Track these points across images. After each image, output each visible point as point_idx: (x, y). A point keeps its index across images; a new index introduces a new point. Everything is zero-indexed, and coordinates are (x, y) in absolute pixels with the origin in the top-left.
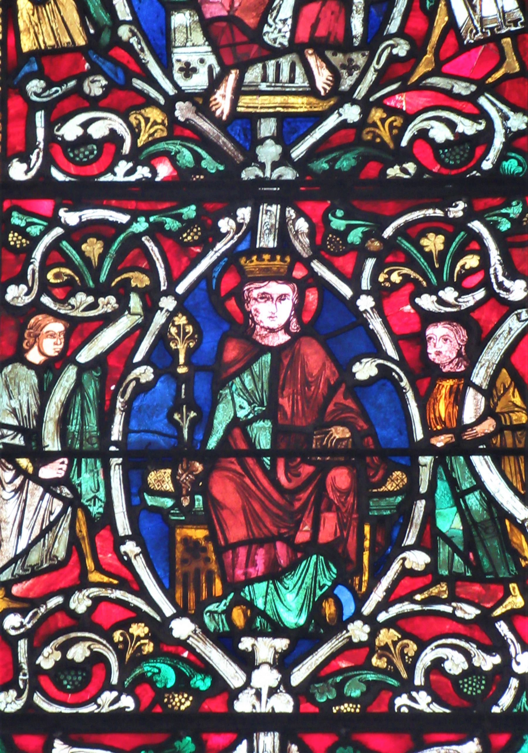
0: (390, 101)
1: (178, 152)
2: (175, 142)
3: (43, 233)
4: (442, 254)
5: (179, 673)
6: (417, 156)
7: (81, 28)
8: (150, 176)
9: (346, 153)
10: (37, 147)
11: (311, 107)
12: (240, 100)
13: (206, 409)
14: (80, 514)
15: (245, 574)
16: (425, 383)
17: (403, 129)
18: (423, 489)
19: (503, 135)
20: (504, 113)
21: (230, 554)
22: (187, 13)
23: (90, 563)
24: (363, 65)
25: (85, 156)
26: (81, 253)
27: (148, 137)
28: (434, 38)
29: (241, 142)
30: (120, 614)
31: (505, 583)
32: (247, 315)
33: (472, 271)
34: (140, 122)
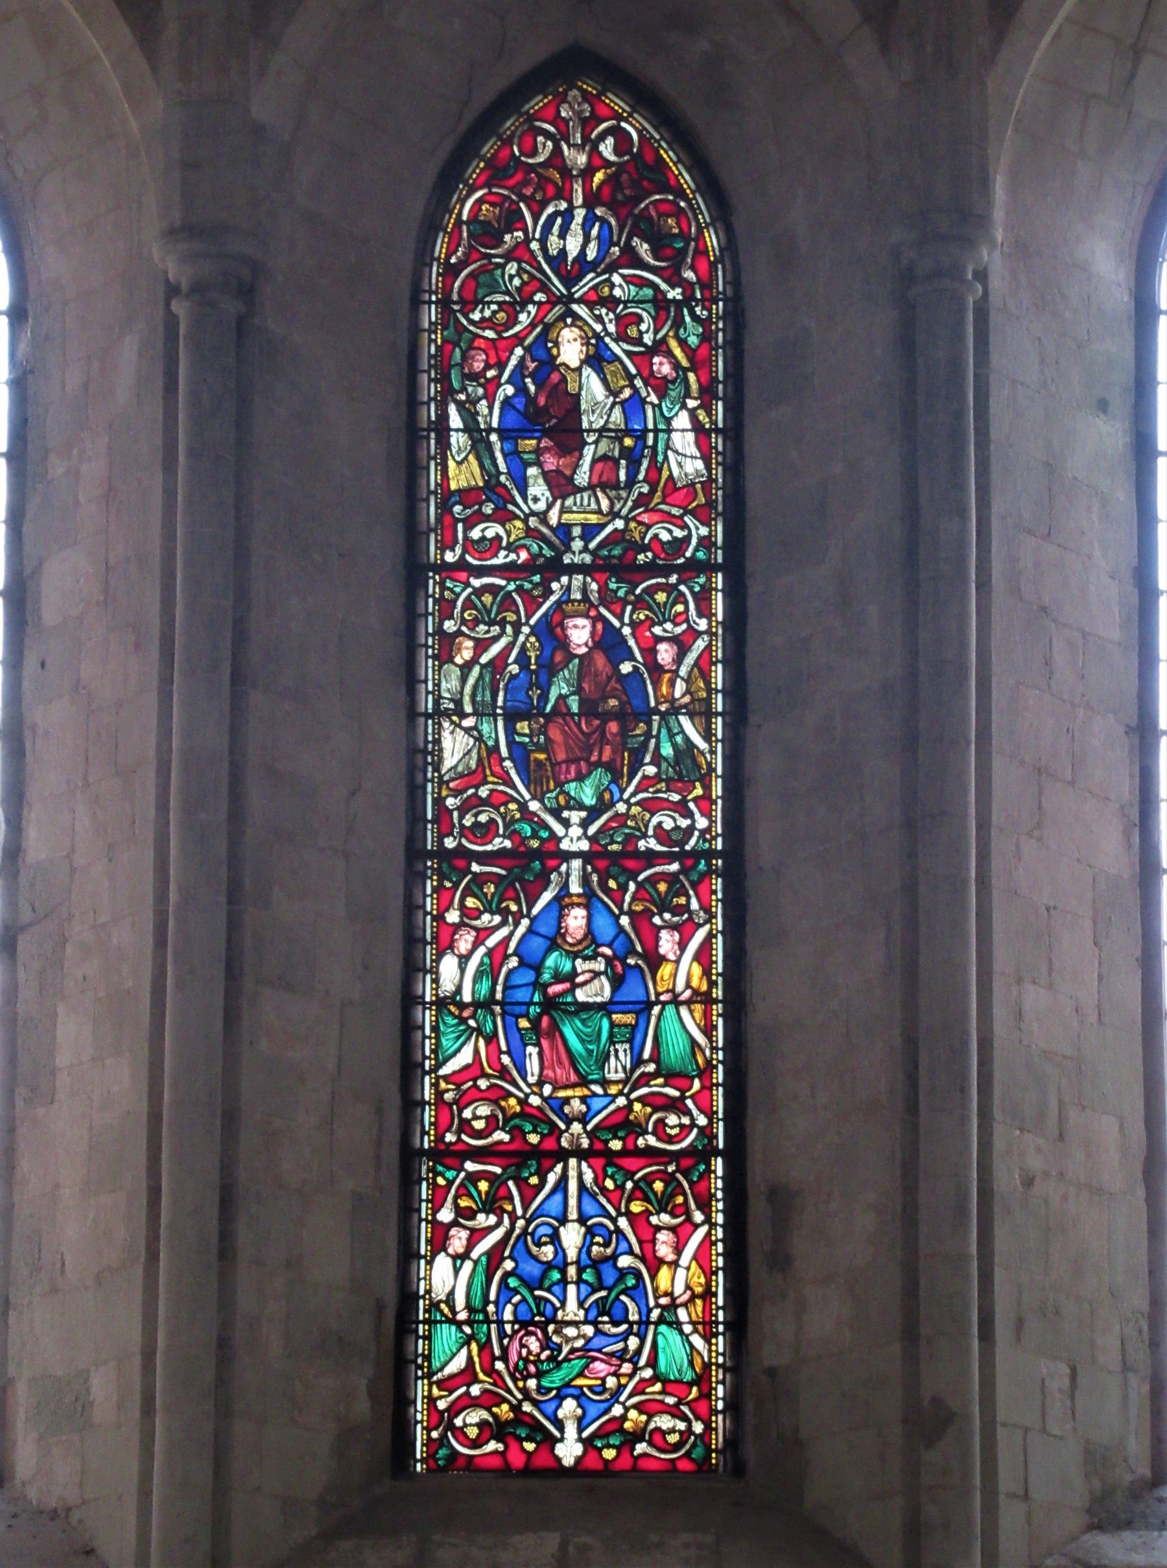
4: (665, 603)
5: (533, 829)
13: (545, 689)
14: (483, 746)
15: (566, 778)
16: (656, 675)
17: (646, 533)
18: (654, 733)
21: (558, 767)
23: (488, 772)
26: (481, 602)
28: (662, 484)
30: (503, 798)
31: (693, 782)
32: (566, 637)
33: (680, 614)
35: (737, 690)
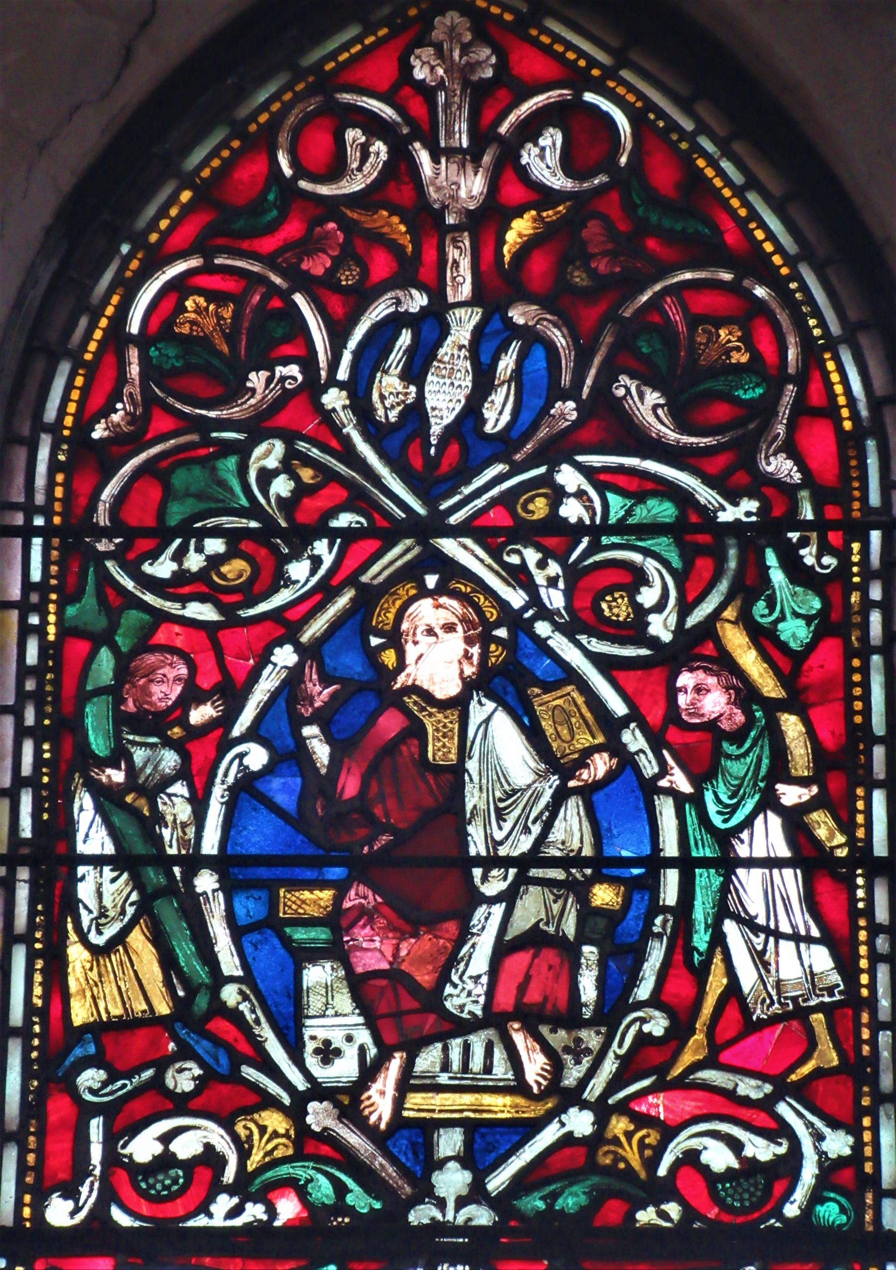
0: (640, 1105)
1: (309, 1181)
2: (306, 1164)
6: (683, 1192)
7: (164, 989)
8: (265, 1217)
9: (572, 1184)
10: (90, 1174)
11: (517, 1112)
12: (408, 1098)
17: (660, 1150)
19: (815, 1164)
20: (816, 1129)
22: (328, 965)
24: (598, 1048)
25: (165, 1188)
27: (264, 1157)
29: (409, 1165)
34: (251, 1133)
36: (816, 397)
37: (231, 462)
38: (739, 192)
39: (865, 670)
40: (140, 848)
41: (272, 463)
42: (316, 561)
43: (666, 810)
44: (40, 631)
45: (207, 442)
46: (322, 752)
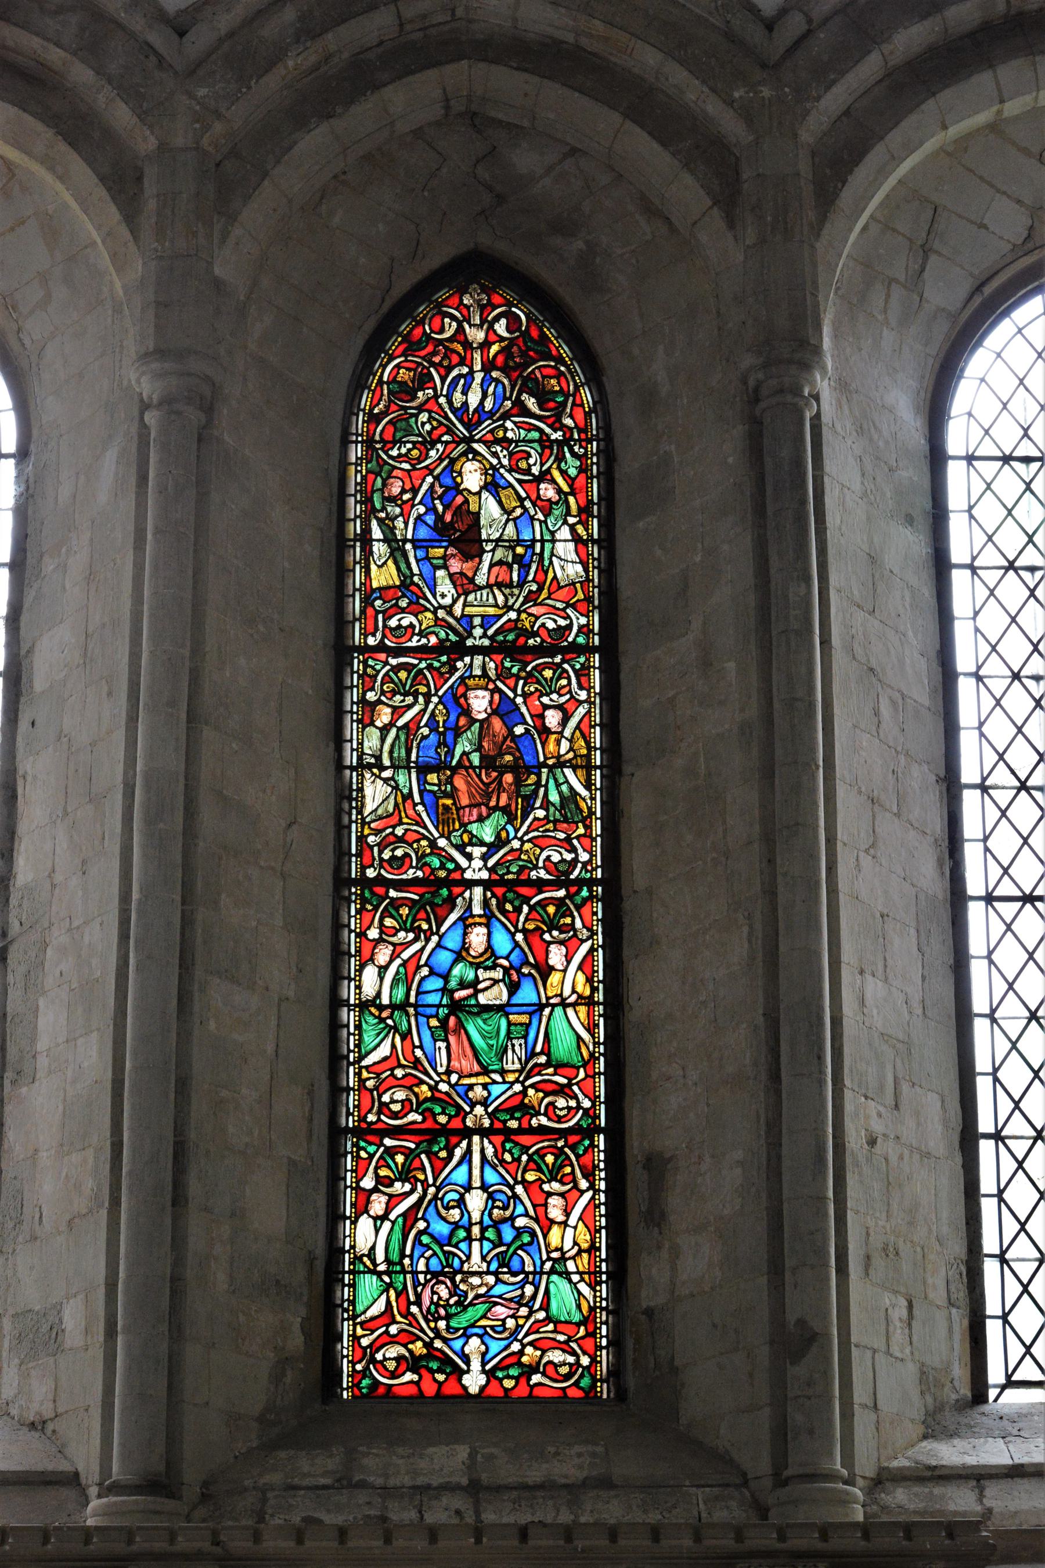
3: (382, 668)
4: (552, 679)
5: (441, 862)
13: (451, 747)
16: (544, 736)
17: (535, 623)
18: (543, 783)
23: (403, 815)
28: (548, 583)
30: (416, 836)
31: (576, 823)
32: (469, 705)
33: (564, 687)
35: (613, 748)
36: (578, 402)
37: (413, 420)
38: (556, 339)
39: (592, 483)
40: (390, 536)
41: (425, 420)
42: (438, 450)
43: (537, 524)
44: (361, 472)
45: (406, 413)
46: (440, 508)
